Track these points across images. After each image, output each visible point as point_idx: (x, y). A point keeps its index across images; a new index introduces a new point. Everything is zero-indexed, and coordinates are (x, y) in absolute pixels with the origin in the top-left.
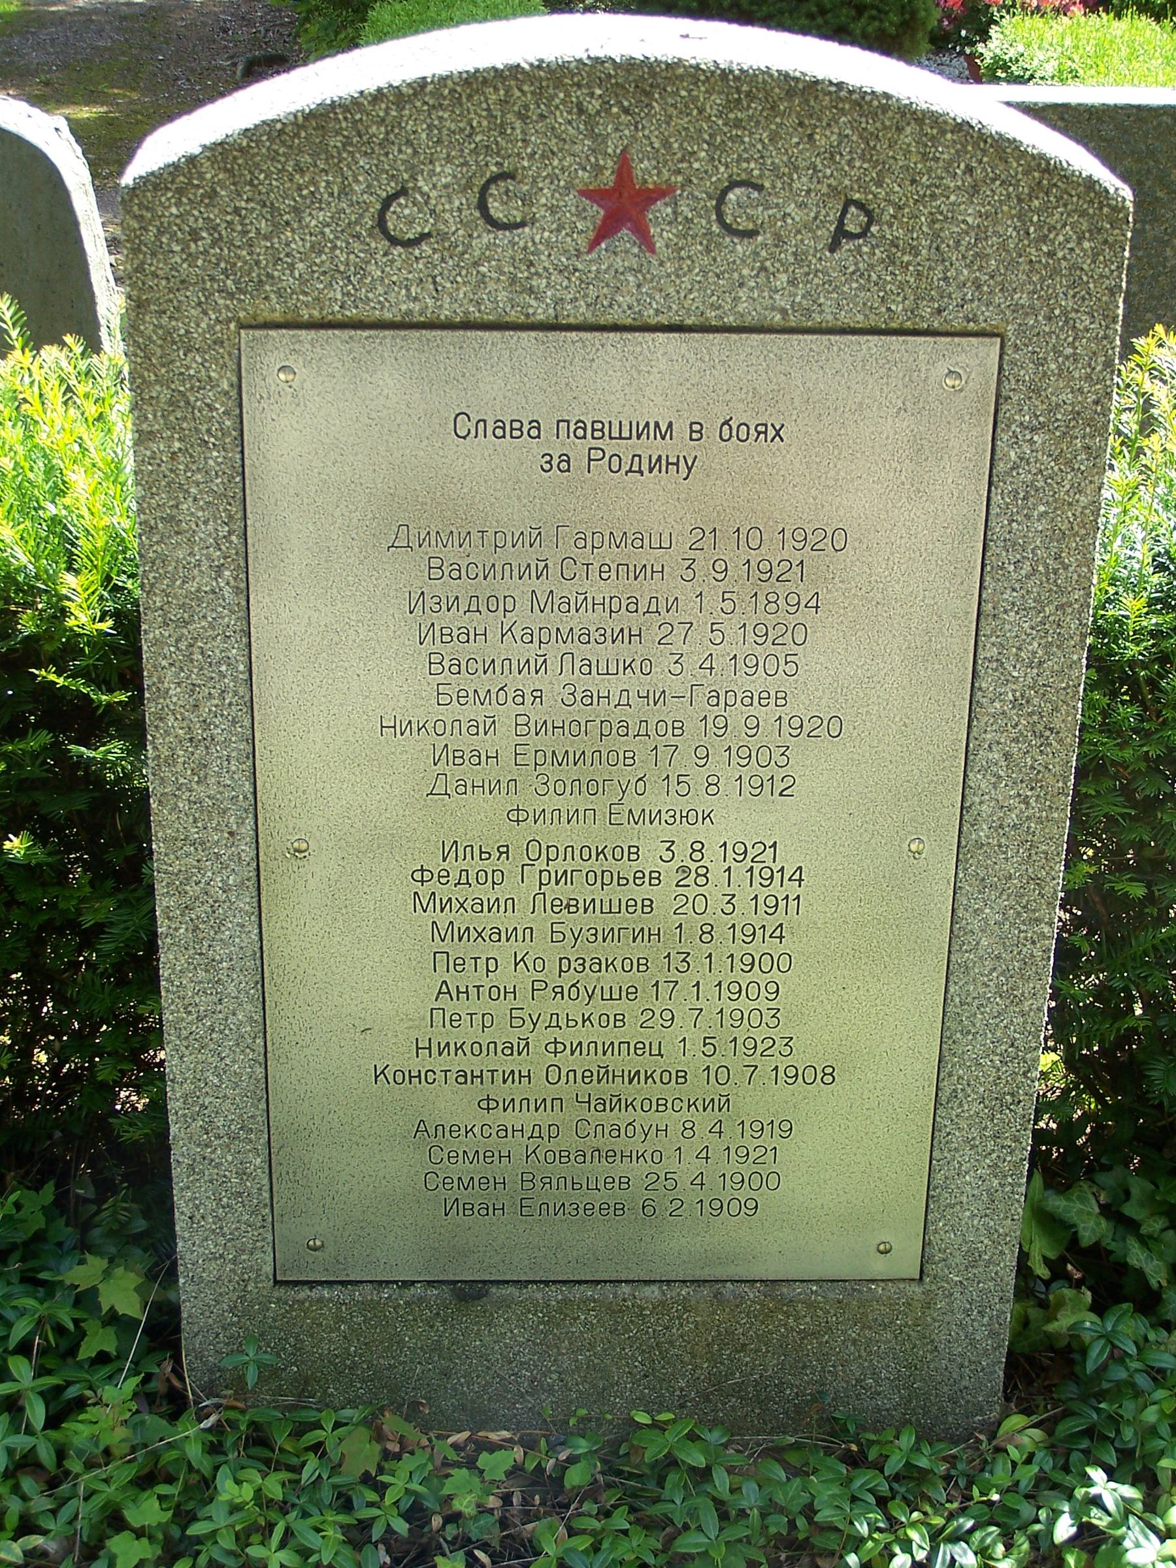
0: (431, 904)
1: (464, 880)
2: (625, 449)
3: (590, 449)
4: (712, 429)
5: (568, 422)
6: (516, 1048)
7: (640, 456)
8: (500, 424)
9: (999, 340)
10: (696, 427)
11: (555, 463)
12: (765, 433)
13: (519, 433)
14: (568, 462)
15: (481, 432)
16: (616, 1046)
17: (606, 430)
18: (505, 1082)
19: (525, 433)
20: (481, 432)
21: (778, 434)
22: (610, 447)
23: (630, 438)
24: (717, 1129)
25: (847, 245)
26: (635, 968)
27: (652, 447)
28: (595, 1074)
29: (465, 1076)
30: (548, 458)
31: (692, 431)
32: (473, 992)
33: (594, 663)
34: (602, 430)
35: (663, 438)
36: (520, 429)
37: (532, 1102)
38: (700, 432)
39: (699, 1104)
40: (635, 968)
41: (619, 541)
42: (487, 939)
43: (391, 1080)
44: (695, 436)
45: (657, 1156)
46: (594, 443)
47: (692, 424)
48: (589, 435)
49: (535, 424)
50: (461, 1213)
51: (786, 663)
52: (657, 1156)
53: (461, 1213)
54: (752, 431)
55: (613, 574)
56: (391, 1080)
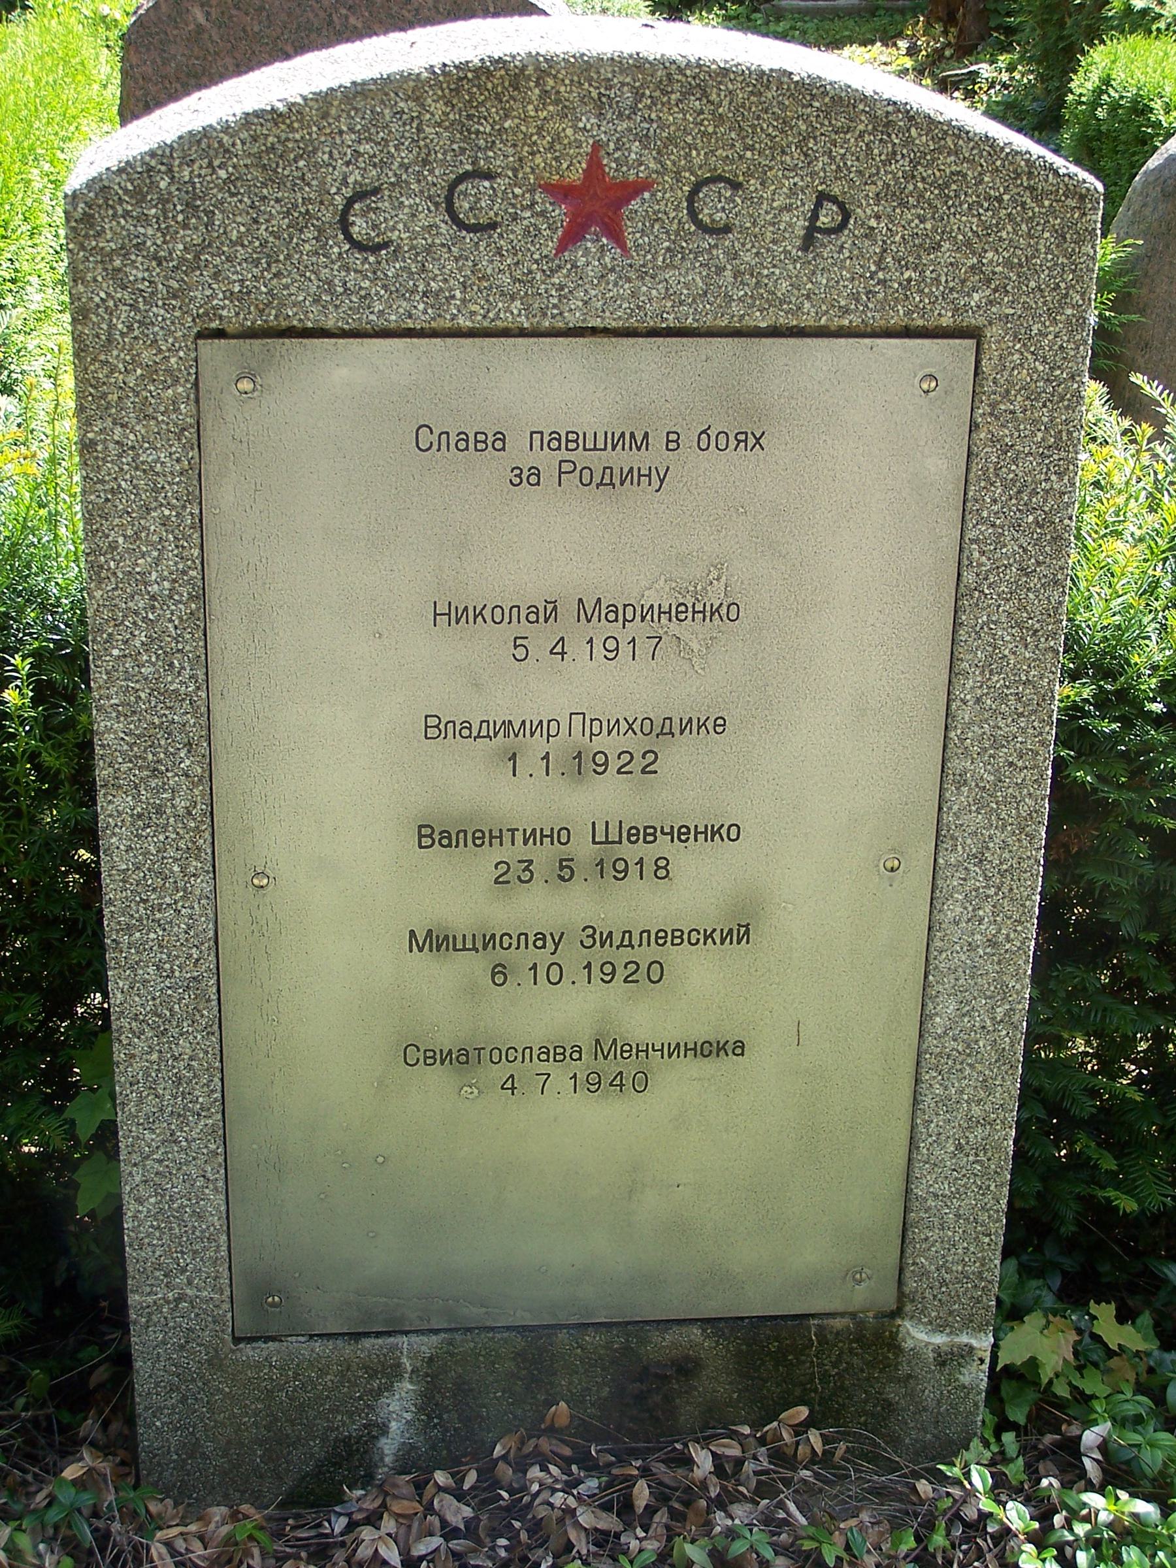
1: (607, 480)
2: (597, 461)
3: (561, 462)
5: (542, 433)
6: (541, 615)
7: (611, 468)
8: (463, 436)
9: (974, 341)
12: (746, 441)
13: (484, 446)
14: (503, 441)
15: (515, 619)
16: (609, 446)
17: (581, 441)
18: (525, 843)
19: (490, 444)
20: (515, 619)
21: (758, 440)
22: (581, 458)
23: (605, 449)
24: (509, 1085)
27: (623, 459)
28: (541, 610)
30: (518, 472)
31: (668, 441)
32: (507, 836)
34: (576, 441)
35: (639, 449)
36: (485, 442)
38: (676, 441)
39: (717, 936)
41: (617, 441)
44: (673, 437)
45: (734, 829)
47: (668, 433)
48: (471, 446)
49: (500, 436)
50: (619, 1056)
52: (734, 829)
54: (732, 438)
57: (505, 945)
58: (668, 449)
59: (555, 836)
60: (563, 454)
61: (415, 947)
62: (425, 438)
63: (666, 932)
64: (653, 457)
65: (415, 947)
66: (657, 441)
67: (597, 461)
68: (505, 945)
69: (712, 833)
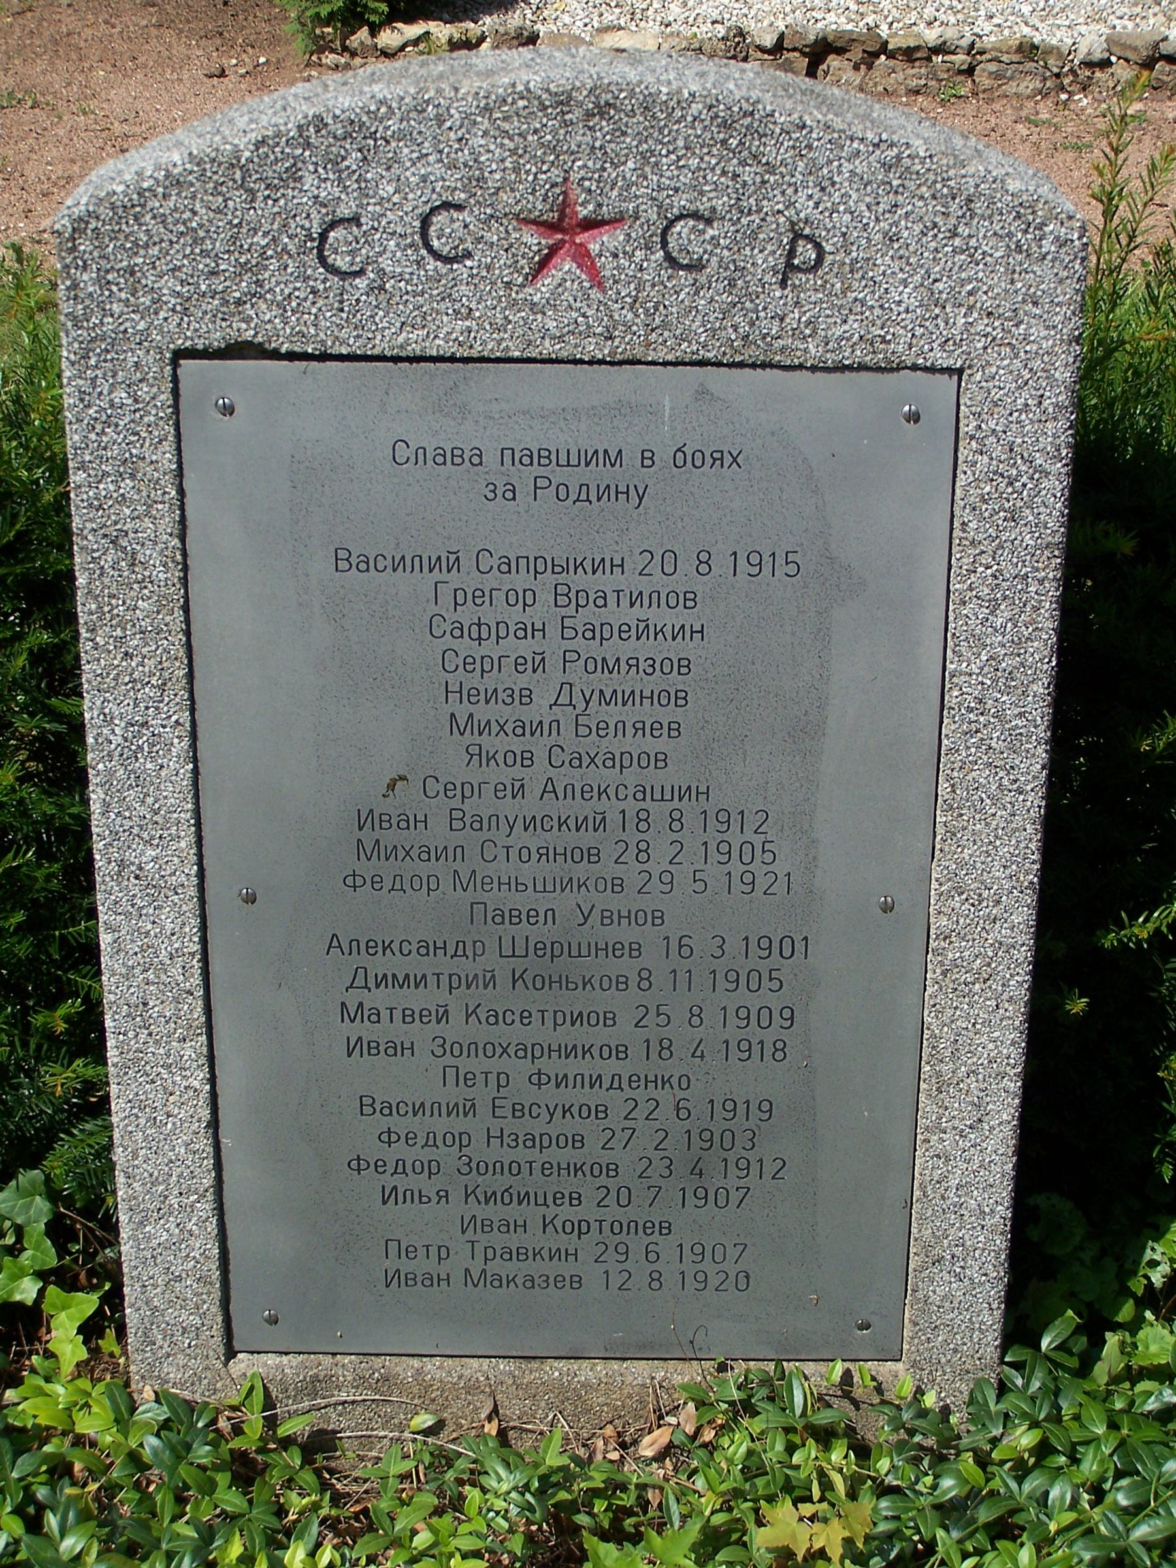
0: (375, 853)
2: (574, 477)
4: (664, 455)
10: (645, 974)
11: (520, 1141)
12: (722, 459)
14: (480, 456)
17: (554, 458)
21: (735, 460)
22: (559, 475)
25: (798, 278)
26: (601, 1022)
27: (598, 475)
29: (427, 948)
33: (648, 790)
34: (548, 457)
36: (461, 456)
37: (587, 1080)
39: (571, 823)
40: (601, 1022)
42: (600, 764)
43: (560, 1229)
45: (684, 1079)
46: (542, 471)
50: (377, 826)
51: (771, 979)
52: (684, 1079)
53: (377, 826)
55: (541, 919)
56: (560, 1229)
57: (509, 1021)
58: (602, 924)
59: (633, 917)
60: (536, 470)
61: (606, 670)
62: (402, 452)
63: (645, 1232)
64: (627, 474)
65: (606, 670)
66: (631, 458)
67: (574, 477)
68: (509, 1021)
69: (718, 459)
